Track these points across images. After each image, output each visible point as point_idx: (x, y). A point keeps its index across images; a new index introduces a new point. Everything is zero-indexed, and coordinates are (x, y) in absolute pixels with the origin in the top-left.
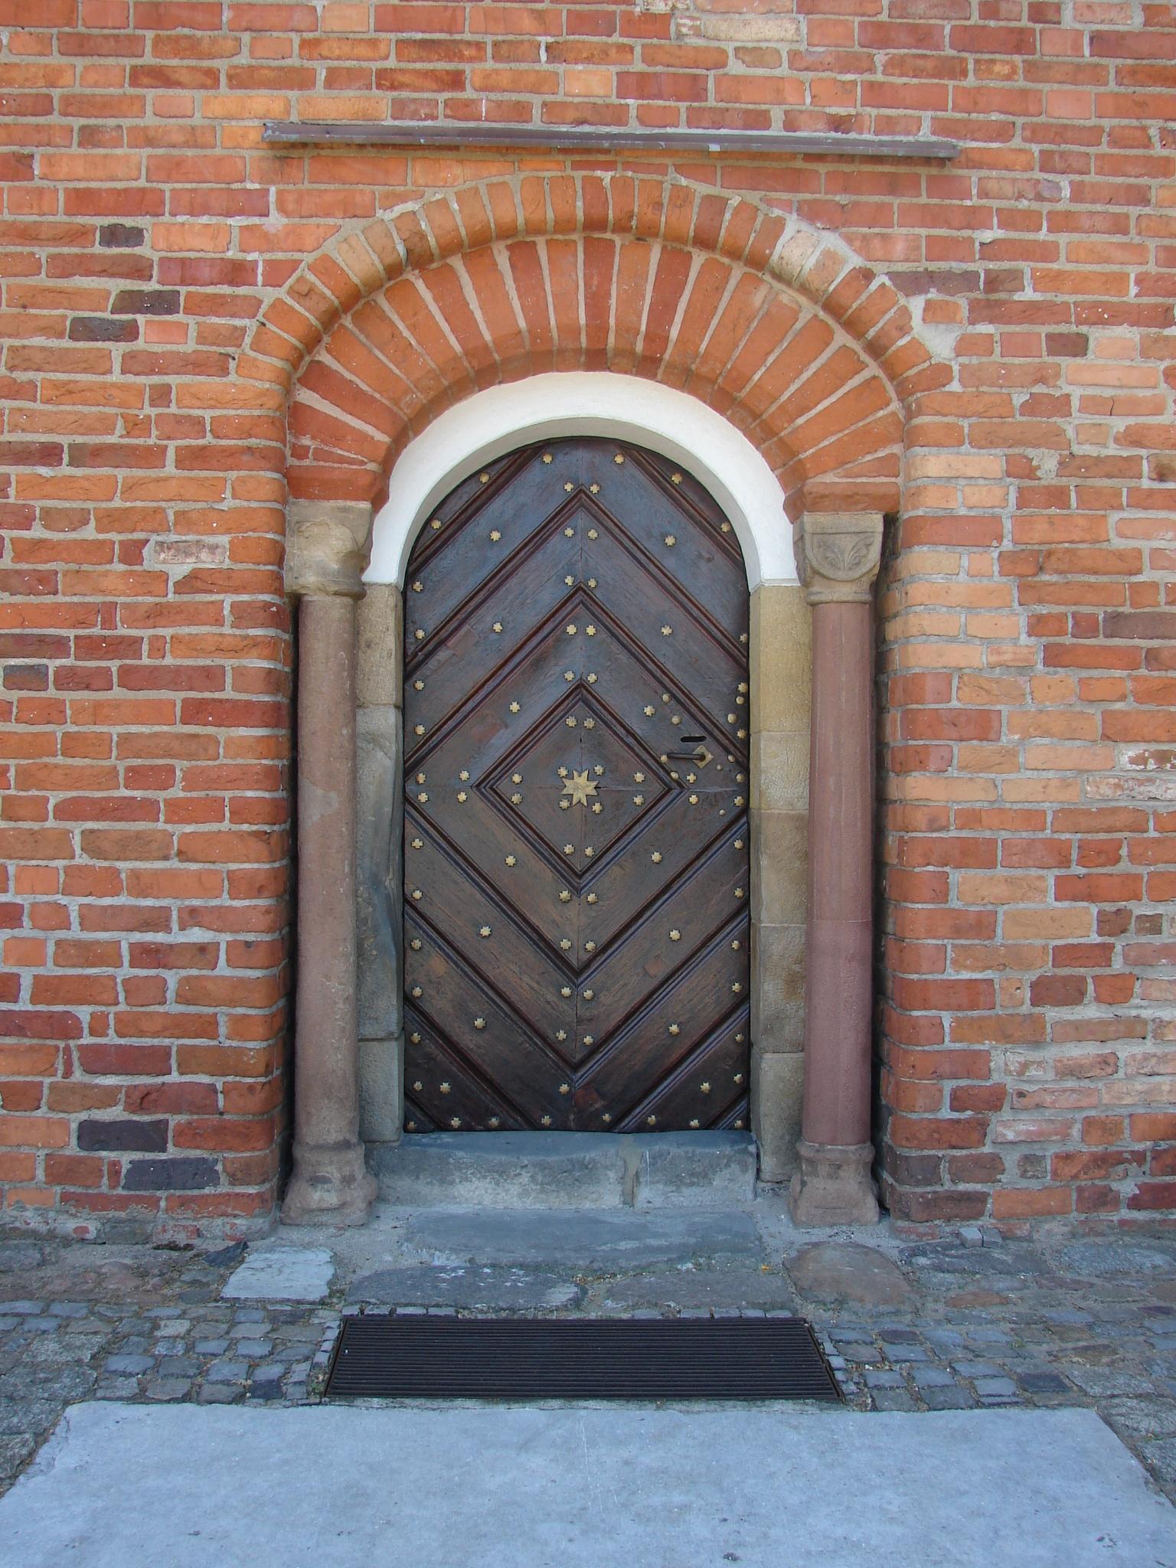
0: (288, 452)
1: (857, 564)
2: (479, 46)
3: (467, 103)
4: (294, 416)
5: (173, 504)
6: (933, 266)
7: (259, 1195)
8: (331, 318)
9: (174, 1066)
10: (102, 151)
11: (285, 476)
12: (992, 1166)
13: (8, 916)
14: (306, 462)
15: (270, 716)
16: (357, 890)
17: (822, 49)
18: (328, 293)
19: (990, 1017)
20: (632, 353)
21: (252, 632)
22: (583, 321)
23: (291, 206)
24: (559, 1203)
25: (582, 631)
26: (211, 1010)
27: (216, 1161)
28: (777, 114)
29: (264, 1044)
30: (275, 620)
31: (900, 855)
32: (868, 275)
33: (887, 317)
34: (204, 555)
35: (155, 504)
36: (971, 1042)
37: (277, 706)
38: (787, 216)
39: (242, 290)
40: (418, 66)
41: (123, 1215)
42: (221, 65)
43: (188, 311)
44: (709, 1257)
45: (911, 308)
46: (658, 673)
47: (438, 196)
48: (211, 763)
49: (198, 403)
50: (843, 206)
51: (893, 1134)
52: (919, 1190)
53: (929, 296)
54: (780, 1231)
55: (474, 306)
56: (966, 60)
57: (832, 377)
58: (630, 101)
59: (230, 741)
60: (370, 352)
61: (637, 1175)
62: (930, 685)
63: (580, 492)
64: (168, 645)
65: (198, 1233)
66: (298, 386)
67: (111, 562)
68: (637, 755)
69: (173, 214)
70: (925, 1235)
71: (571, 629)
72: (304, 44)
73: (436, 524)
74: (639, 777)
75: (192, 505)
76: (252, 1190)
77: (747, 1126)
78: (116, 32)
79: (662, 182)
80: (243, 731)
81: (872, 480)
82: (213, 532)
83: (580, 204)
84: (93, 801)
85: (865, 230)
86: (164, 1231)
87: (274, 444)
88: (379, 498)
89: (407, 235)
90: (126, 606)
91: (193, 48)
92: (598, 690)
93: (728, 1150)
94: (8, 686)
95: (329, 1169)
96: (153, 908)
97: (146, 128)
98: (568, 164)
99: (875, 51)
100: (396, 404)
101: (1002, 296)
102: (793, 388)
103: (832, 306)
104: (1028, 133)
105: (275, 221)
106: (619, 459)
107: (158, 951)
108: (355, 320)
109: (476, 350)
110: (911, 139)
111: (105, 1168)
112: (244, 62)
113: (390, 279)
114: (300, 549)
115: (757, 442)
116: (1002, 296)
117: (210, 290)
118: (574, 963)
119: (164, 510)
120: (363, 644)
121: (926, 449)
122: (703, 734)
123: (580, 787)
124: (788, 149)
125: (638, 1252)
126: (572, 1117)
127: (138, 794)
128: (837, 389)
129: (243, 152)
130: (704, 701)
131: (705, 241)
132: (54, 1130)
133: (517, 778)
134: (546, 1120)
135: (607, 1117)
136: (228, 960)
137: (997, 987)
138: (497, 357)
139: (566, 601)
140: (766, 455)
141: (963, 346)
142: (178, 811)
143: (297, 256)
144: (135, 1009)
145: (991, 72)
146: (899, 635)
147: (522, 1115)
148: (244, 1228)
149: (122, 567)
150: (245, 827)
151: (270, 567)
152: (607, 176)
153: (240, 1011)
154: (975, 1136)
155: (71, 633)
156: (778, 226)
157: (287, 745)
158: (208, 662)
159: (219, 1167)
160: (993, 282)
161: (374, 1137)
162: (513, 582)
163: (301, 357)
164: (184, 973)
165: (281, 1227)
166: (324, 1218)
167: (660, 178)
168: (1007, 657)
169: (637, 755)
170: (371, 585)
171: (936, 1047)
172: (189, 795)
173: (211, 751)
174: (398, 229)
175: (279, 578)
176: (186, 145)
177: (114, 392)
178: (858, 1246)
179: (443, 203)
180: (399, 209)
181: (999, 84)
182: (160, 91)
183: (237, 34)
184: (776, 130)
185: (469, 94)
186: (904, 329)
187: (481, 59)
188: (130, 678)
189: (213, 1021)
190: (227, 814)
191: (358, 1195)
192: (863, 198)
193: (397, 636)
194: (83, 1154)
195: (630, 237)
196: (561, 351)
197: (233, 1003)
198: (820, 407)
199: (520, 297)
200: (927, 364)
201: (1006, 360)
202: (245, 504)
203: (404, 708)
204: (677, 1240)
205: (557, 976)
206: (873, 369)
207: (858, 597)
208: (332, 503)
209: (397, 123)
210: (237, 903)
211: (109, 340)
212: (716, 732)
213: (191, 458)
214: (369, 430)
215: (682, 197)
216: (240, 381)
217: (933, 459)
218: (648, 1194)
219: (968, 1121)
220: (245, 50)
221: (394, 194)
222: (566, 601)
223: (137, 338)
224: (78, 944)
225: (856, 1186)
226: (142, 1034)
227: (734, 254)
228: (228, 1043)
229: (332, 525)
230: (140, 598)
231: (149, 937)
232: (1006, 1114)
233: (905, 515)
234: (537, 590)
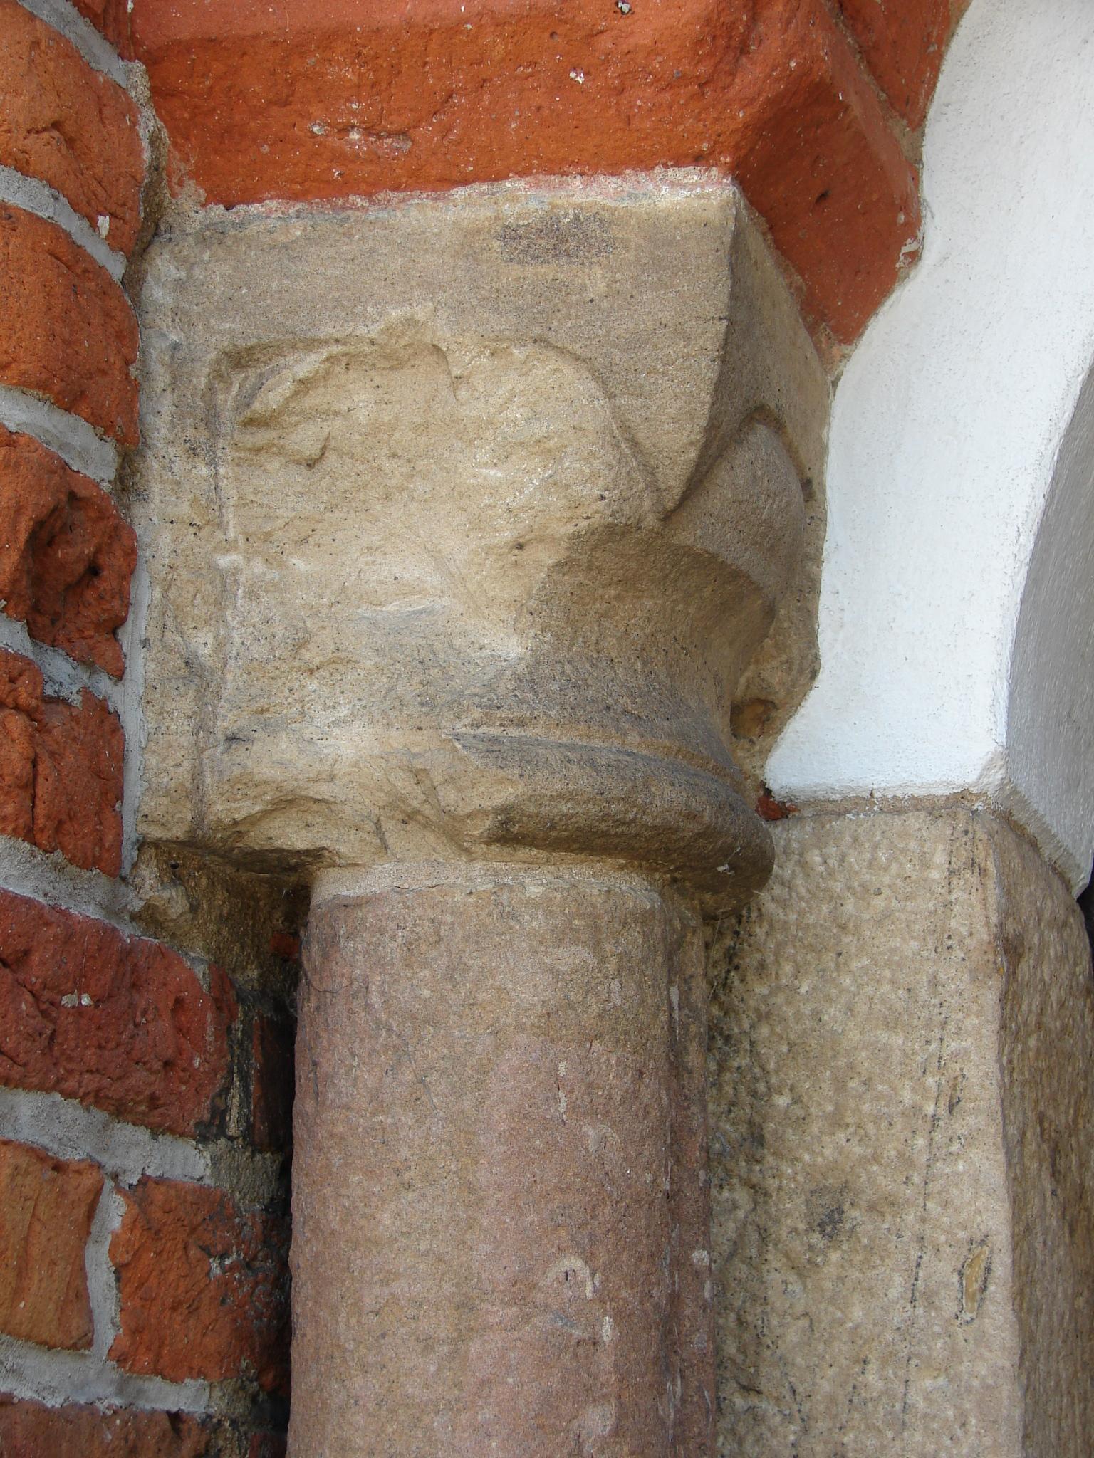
114: (258, 540)
120: (792, 1212)
208: (468, 206)
229: (466, 358)
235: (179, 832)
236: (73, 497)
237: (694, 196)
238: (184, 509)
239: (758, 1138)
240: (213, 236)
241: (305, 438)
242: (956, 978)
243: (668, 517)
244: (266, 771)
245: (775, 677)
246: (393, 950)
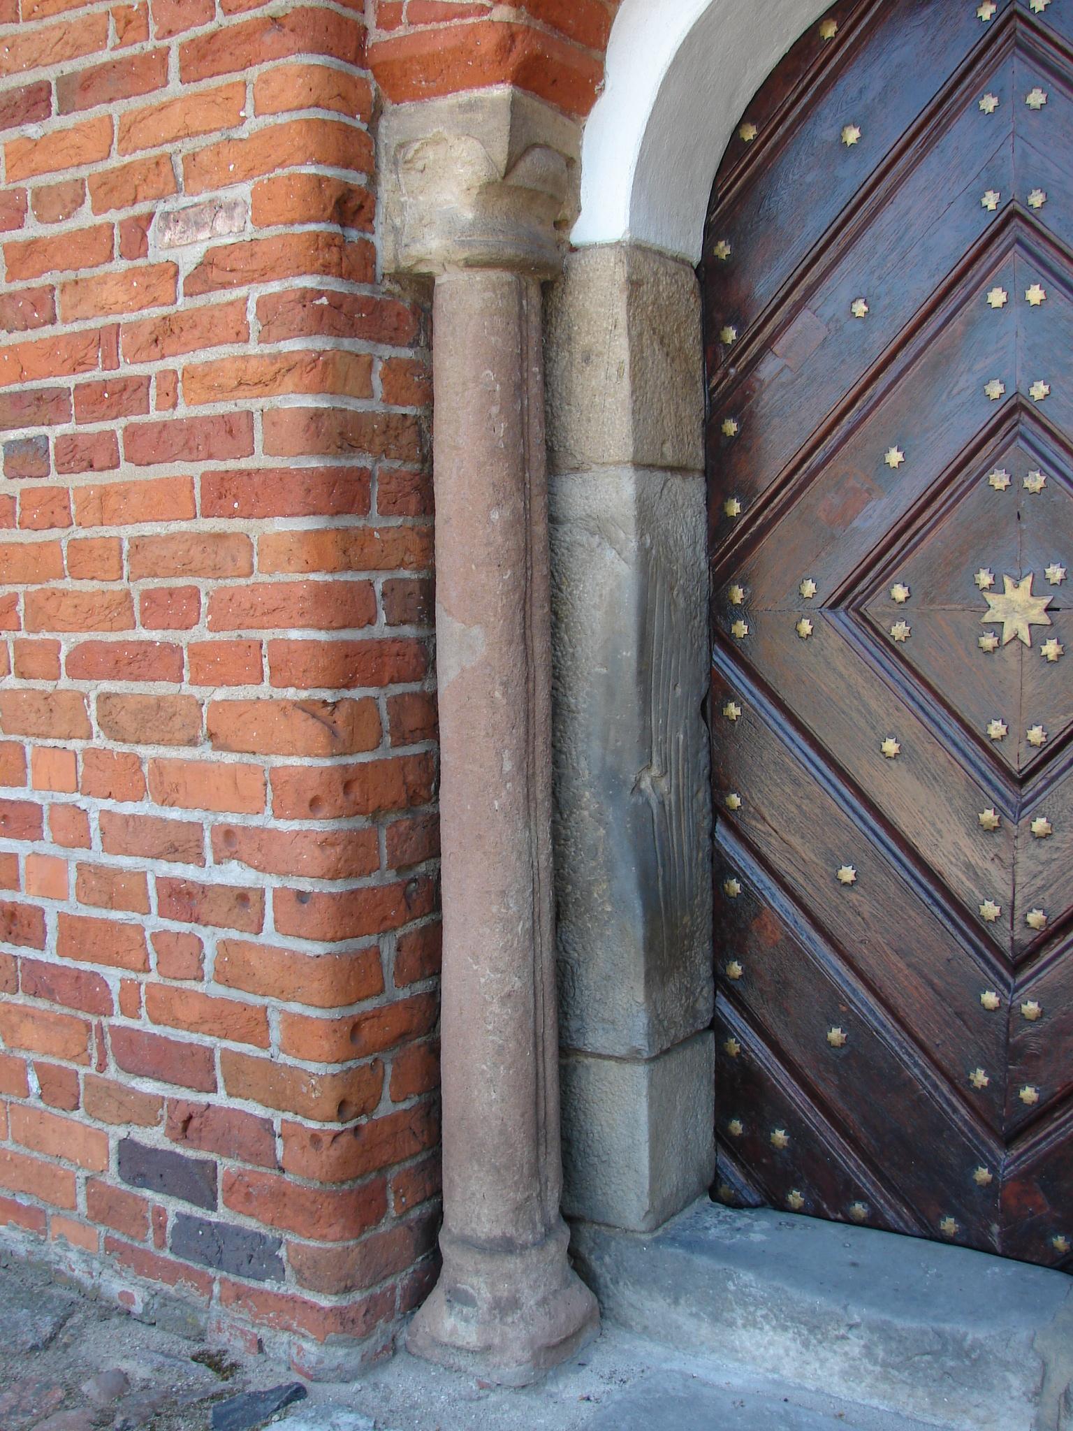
5: (178, 145)
7: (338, 1312)
13: (21, 820)
14: (400, 31)
25: (1016, 297)
26: (256, 1000)
35: (156, 152)
41: (171, 1289)
48: (242, 582)
67: (110, 258)
76: (326, 1302)
82: (229, 182)
84: (108, 648)
92: (1051, 415)
94: (12, 472)
95: (474, 1280)
114: (411, 193)
120: (578, 357)
126: (995, 1228)
127: (156, 636)
132: (88, 1145)
133: (900, 593)
134: (949, 1225)
142: (210, 666)
148: (313, 1359)
150: (291, 693)
151: (312, 227)
155: (69, 382)
161: (612, 1219)
162: (888, 216)
173: (242, 563)
190: (267, 670)
191: (517, 1339)
194: (124, 1187)
208: (452, 99)
224: (99, 871)
226: (176, 1023)
229: (452, 140)
230: (145, 312)
235: (393, 271)
236: (350, 190)
237: (501, 92)
238: (389, 187)
239: (570, 339)
240: (395, 113)
241: (419, 165)
242: (616, 291)
243: (504, 178)
244: (414, 253)
245: (568, 212)
246: (447, 297)
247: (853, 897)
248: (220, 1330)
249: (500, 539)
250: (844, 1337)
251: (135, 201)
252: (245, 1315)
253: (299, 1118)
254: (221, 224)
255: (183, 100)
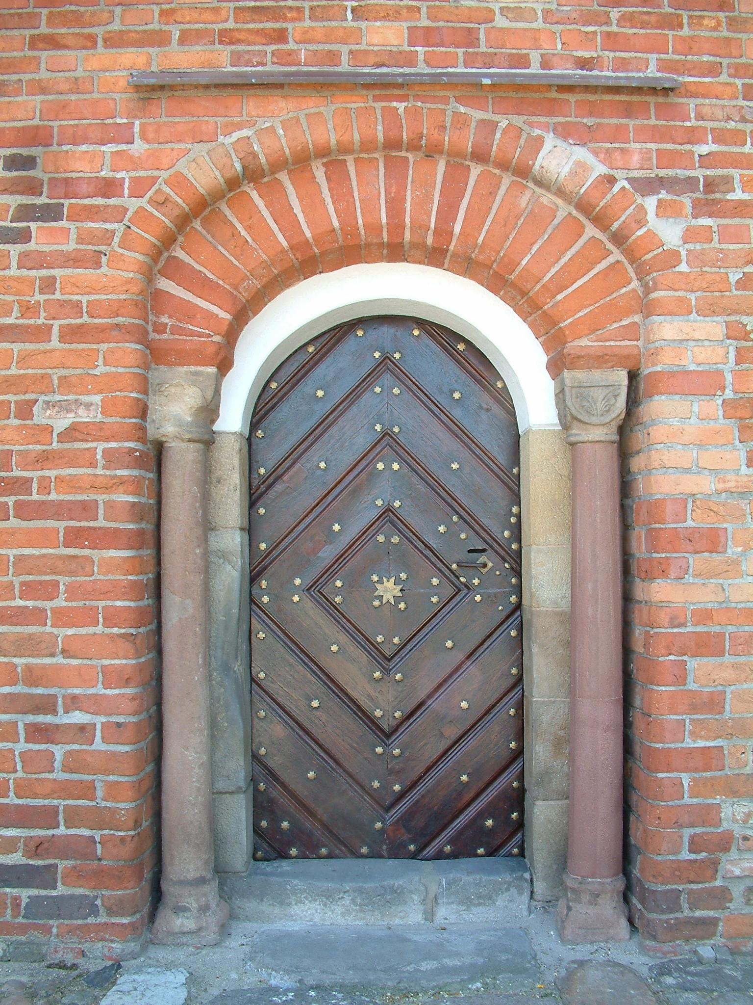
0: (150, 329)
1: (608, 411)
2: (299, 10)
3: (290, 53)
4: (153, 301)
5: (57, 370)
6: (662, 173)
8: (183, 221)
9: (62, 822)
10: (6, 99)
11: (147, 347)
12: (721, 897)
14: (165, 336)
15: (137, 540)
16: (210, 676)
17: (569, 8)
18: (180, 201)
19: (720, 777)
20: (424, 245)
21: (119, 472)
22: (384, 220)
23: (151, 135)
24: (373, 921)
25: (388, 467)
26: (89, 778)
27: (96, 897)
28: (535, 57)
29: (133, 805)
30: (140, 462)
31: (646, 645)
32: (612, 180)
33: (628, 212)
34: (81, 411)
35: (43, 371)
36: (705, 797)
37: (141, 533)
38: (545, 134)
39: (113, 201)
40: (252, 26)
41: (23, 938)
42: (99, 31)
43: (69, 219)
44: (494, 978)
45: (646, 205)
46: (449, 500)
47: (267, 125)
49: (77, 291)
50: (590, 127)
51: (642, 870)
52: (664, 917)
53: (661, 196)
54: (552, 949)
55: (298, 210)
56: (681, 15)
57: (584, 262)
58: (418, 49)
59: (102, 560)
60: (215, 248)
61: (436, 898)
62: (669, 508)
63: (386, 358)
64: (52, 484)
65: (83, 954)
66: (158, 276)
68: (433, 564)
69: (60, 145)
70: (669, 952)
71: (380, 466)
72: (163, 13)
73: (274, 385)
74: (435, 581)
75: (71, 372)
76: (125, 921)
77: (522, 854)
78: (20, 11)
79: (445, 110)
80: (112, 553)
81: (618, 343)
82: (88, 393)
83: (380, 128)
85: (608, 145)
86: (56, 952)
87: (136, 321)
88: (225, 365)
89: (242, 155)
90: (20, 452)
91: (77, 20)
92: (402, 513)
93: (508, 878)
96: (43, 695)
97: (40, 80)
98: (370, 97)
99: (610, 9)
100: (236, 289)
101: (718, 196)
102: (553, 271)
103: (584, 206)
104: (732, 71)
105: (139, 147)
106: (416, 332)
107: (46, 730)
108: (203, 224)
109: (299, 245)
110: (641, 75)
111: (9, 902)
112: (116, 28)
113: (230, 191)
114: (160, 405)
115: (524, 315)
116: (718, 196)
117: (87, 201)
118: (385, 727)
119: (50, 376)
120: (214, 480)
121: (662, 317)
122: (485, 546)
123: (388, 590)
124: (545, 82)
125: (436, 972)
127: (30, 604)
128: (588, 271)
129: (114, 96)
130: (485, 521)
131: (480, 156)
135: (412, 847)
136: (103, 738)
137: (726, 752)
138: (316, 250)
139: (376, 444)
140: (532, 326)
141: (689, 236)
142: (62, 617)
143: (156, 173)
144: (29, 776)
145: (701, 25)
146: (643, 467)
147: (345, 846)
148: (119, 950)
149: (17, 422)
150: (115, 630)
151: (134, 420)
152: (401, 106)
153: (113, 778)
154: (709, 873)
156: (539, 142)
157: (153, 562)
158: (84, 497)
159: (99, 902)
160: (710, 185)
162: (334, 429)
163: (160, 253)
164: (68, 747)
165: (151, 946)
166: (184, 939)
167: (443, 107)
168: (732, 484)
169: (433, 564)
170: (220, 433)
171: (677, 802)
172: (70, 604)
173: (88, 569)
174: (236, 151)
175: (143, 429)
176: (71, 91)
177: (12, 283)
178: (617, 964)
179: (272, 129)
180: (236, 135)
181: (708, 34)
182: (51, 53)
183: (111, 8)
184: (535, 69)
185: (291, 46)
186: (641, 222)
187: (300, 19)
188: (24, 511)
189: (92, 786)
190: (101, 620)
191: (212, 921)
192: (605, 121)
193: (242, 472)
195: (421, 154)
196: (368, 245)
197: (107, 772)
198: (575, 286)
199: (333, 203)
200: (661, 250)
201: (723, 246)
202: (114, 370)
203: (251, 529)
204: (468, 960)
205: (371, 737)
206: (616, 255)
207: (608, 438)
209: (234, 69)
210: (109, 692)
211: (9, 243)
212: (495, 545)
213: (71, 334)
214: (215, 310)
215: (461, 121)
216: (111, 272)
217: (667, 326)
218: (445, 913)
219: (702, 861)
220: (117, 20)
221: (233, 124)
222: (376, 444)
223: (30, 241)
225: (612, 911)
226: (35, 796)
227: (504, 165)
228: (104, 804)
230: (31, 447)
231: (40, 719)
232: (733, 854)
233: (645, 371)
234: (354, 435)
240: (156, 369)
241: (166, 394)
247: (317, 713)
248: (56, 952)
249: (200, 561)
250: (343, 898)
251: (26, 392)
252: (75, 939)
253: (112, 832)
254: (81, 411)
255: (60, 351)
